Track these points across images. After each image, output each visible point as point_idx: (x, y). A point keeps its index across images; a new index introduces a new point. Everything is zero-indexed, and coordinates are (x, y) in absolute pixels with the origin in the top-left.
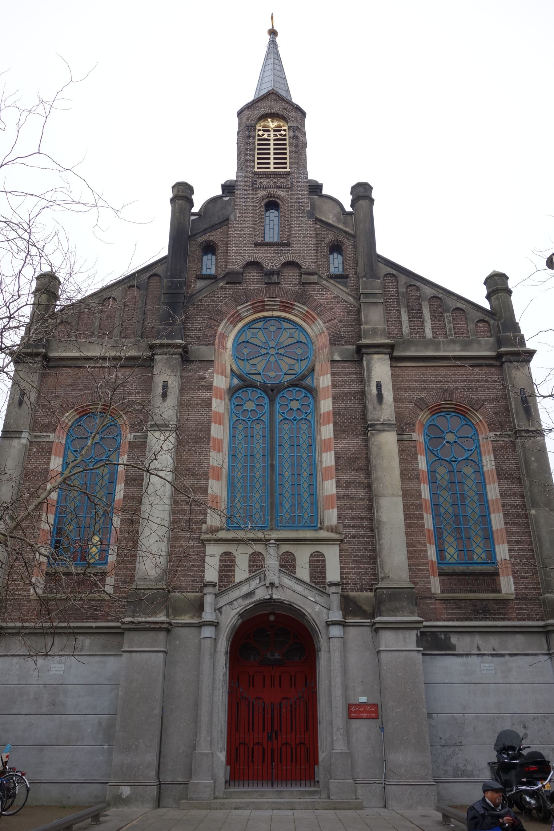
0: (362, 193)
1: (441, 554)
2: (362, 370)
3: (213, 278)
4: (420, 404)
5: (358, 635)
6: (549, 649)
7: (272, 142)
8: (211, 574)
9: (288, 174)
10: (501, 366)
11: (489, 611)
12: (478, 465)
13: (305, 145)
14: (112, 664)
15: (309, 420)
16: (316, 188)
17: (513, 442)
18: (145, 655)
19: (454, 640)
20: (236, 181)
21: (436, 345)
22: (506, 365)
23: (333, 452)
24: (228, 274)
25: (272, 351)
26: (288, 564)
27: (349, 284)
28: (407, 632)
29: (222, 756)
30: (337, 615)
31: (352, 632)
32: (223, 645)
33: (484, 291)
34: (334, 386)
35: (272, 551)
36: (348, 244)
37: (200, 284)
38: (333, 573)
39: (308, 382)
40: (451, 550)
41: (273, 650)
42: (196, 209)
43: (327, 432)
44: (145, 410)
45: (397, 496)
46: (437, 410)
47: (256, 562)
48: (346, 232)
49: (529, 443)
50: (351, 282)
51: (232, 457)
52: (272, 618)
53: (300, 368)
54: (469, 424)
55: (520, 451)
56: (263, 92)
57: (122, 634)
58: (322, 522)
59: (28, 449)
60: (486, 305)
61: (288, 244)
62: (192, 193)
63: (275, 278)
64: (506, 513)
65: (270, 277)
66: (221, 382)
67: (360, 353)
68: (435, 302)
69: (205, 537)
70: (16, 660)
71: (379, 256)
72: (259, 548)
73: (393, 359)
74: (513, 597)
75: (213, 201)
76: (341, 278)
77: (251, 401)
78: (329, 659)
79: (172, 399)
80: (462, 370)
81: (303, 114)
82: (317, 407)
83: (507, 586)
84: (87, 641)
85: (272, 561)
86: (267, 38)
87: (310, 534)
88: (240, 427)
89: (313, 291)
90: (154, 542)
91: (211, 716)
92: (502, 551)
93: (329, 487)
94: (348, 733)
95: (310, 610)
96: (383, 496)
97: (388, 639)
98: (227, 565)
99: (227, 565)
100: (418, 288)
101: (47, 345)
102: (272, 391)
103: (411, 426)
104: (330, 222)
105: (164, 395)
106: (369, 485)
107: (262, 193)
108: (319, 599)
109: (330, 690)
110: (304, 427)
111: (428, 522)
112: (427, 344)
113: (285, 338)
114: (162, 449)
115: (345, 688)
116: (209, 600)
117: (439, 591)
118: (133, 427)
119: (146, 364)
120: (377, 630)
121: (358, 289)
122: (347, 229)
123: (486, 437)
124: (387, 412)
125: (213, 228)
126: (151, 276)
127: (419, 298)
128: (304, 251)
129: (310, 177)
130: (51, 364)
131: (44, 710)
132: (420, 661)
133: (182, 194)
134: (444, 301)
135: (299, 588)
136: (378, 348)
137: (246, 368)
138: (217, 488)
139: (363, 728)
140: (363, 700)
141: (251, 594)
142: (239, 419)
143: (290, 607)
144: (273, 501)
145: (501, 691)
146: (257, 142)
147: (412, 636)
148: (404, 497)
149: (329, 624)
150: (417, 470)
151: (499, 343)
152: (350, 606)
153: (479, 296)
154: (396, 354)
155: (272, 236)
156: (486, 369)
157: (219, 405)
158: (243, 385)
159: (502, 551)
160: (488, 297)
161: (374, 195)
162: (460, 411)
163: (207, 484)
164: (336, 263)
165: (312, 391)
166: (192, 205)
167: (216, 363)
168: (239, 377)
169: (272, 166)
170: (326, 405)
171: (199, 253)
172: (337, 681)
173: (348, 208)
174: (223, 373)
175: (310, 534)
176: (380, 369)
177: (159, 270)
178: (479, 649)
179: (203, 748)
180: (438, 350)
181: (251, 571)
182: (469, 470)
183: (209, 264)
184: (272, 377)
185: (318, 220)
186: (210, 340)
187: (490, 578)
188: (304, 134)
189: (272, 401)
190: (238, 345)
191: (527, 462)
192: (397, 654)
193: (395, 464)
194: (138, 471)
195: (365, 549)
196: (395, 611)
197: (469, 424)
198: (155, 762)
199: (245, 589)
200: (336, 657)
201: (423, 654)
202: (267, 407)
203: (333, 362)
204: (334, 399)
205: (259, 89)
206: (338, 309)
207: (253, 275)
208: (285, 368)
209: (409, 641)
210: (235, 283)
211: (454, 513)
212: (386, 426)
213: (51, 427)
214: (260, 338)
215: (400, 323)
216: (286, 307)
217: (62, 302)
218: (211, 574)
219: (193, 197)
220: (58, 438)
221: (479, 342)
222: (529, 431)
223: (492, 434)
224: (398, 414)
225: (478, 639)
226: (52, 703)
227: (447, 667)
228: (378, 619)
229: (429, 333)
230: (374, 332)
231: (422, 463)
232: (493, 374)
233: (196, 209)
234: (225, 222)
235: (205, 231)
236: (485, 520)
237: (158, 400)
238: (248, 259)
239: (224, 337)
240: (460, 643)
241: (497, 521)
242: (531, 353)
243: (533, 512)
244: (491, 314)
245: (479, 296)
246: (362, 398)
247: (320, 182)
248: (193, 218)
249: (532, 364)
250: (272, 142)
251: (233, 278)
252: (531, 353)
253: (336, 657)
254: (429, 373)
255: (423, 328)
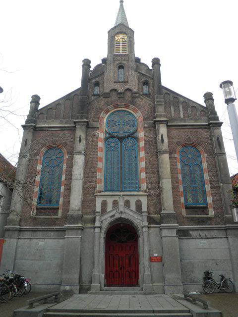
0: (156, 62)
1: (186, 200)
2: (156, 130)
3: (98, 96)
4: (178, 143)
5: (154, 231)
6: (226, 235)
7: (121, 43)
8: (98, 208)
9: (127, 55)
10: (210, 128)
11: (204, 222)
12: (200, 167)
13: (134, 43)
14: (61, 241)
15: (135, 150)
16: (138, 60)
17: (214, 157)
18: (74, 239)
19: (191, 232)
20: (107, 58)
21: (184, 120)
22: (211, 128)
23: (144, 162)
24: (104, 94)
25: (121, 124)
26: (127, 204)
27: (151, 97)
28: (173, 230)
29: (103, 276)
30: (146, 224)
31: (152, 230)
32: (103, 235)
33: (203, 99)
34: (145, 137)
35: (121, 199)
36: (151, 82)
37: (93, 98)
38: (145, 208)
39: (135, 135)
40: (190, 199)
41: (122, 236)
42: (92, 69)
43: (142, 154)
44: (73, 147)
45: (169, 178)
46: (185, 146)
47: (115, 203)
48: (149, 77)
49: (220, 158)
50: (152, 96)
51: (106, 164)
52: (122, 225)
53: (132, 130)
54: (197, 150)
55: (217, 160)
56: (118, 24)
57: (65, 231)
58: (140, 188)
59: (29, 161)
60: (204, 105)
61: (127, 82)
62: (90, 63)
63: (122, 95)
64: (211, 184)
65: (121, 95)
66: (101, 135)
67: (155, 124)
68: (184, 104)
69: (96, 194)
70: (26, 240)
71: (162, 86)
72: (117, 199)
73: (168, 126)
74: (213, 216)
75: (99, 65)
76: (148, 95)
77: (113, 143)
78: (143, 240)
79: (83, 143)
80: (194, 130)
81: (133, 32)
82: (139, 145)
83: (211, 212)
84: (52, 234)
85: (121, 203)
86: (119, 4)
87: (136, 193)
88: (110, 153)
89: (137, 100)
90: (76, 201)
91: (99, 261)
92: (210, 200)
93: (143, 175)
94: (150, 267)
95: (135, 222)
96: (163, 178)
97: (165, 233)
98: (104, 204)
99: (104, 204)
100: (178, 99)
101: (35, 122)
102: (121, 139)
103: (175, 152)
104: (144, 73)
105: (80, 141)
106: (158, 174)
107: (117, 62)
108: (140, 218)
109: (143, 251)
110: (133, 152)
111: (181, 188)
112: (181, 120)
113: (126, 119)
114: (79, 160)
115: (149, 251)
116: (97, 218)
117: (185, 214)
118: (68, 153)
119: (73, 129)
120: (161, 229)
121: (154, 99)
122: (150, 76)
123: (204, 156)
124: (165, 146)
125: (98, 76)
126: (74, 95)
127: (178, 102)
128: (134, 86)
129: (136, 56)
130: (37, 129)
131: (37, 258)
132: (178, 241)
133: (87, 63)
134: (188, 104)
135: (131, 214)
136: (161, 122)
137: (111, 130)
138: (100, 176)
139: (156, 265)
140: (156, 255)
141: (113, 216)
142: (108, 149)
143: (128, 220)
144: (122, 180)
145: (208, 250)
146: (115, 43)
147: (175, 231)
148: (172, 179)
149: (143, 227)
150: (177, 168)
151: (209, 119)
152: (151, 220)
153: (201, 101)
154: (169, 124)
155: (121, 79)
156: (204, 129)
157: (101, 144)
158: (110, 137)
159: (210, 200)
160: (205, 102)
161: (214, 97)
162: (194, 146)
163: (96, 174)
164: (146, 89)
165: (137, 139)
166: (90, 68)
167: (99, 128)
168: (109, 134)
169: (121, 52)
170: (142, 144)
171: (93, 86)
172: (146, 248)
173: (151, 68)
174: (102, 132)
175: (136, 193)
176: (163, 130)
177: (77, 93)
178: (200, 236)
179: (96, 273)
180: (185, 122)
181: (113, 207)
182: (197, 168)
183: (97, 91)
184: (121, 134)
185: (139, 73)
186: (97, 119)
187: (205, 209)
188: (134, 39)
189: (121, 143)
190: (108, 121)
191: (219, 165)
192: (169, 238)
193: (168, 166)
194: (70, 166)
195: (157, 200)
196: (168, 222)
197: (197, 150)
198: (78, 277)
199: (111, 214)
200: (146, 239)
201: (179, 238)
202: (119, 145)
203: (145, 127)
204: (145, 141)
205: (116, 23)
206: (147, 108)
207: (114, 94)
208: (126, 130)
209: (174, 233)
210: (106, 97)
211: (190, 181)
212: (165, 152)
213: (37, 154)
214: (117, 119)
215: (171, 112)
216: (127, 106)
217: (40, 107)
218: (98, 208)
219: (91, 64)
220: (40, 158)
221: (201, 119)
222: (221, 153)
223: (206, 155)
224: (169, 147)
225: (200, 232)
226: (38, 256)
227: (191, 244)
228: (162, 225)
229: (182, 116)
230: (161, 116)
231: (179, 166)
232: (207, 132)
233: (92, 69)
234: (103, 73)
235: (95, 77)
236: (203, 187)
237: (78, 142)
238: (112, 88)
239: (103, 118)
240: (194, 234)
241: (208, 188)
242: (221, 124)
243: (221, 184)
244: (206, 108)
245: (201, 101)
246: (156, 141)
247: (139, 58)
248: (91, 72)
249: (222, 127)
250: (121, 43)
251: (106, 95)
252: (221, 124)
253: (146, 239)
254: (182, 131)
255: (180, 114)
